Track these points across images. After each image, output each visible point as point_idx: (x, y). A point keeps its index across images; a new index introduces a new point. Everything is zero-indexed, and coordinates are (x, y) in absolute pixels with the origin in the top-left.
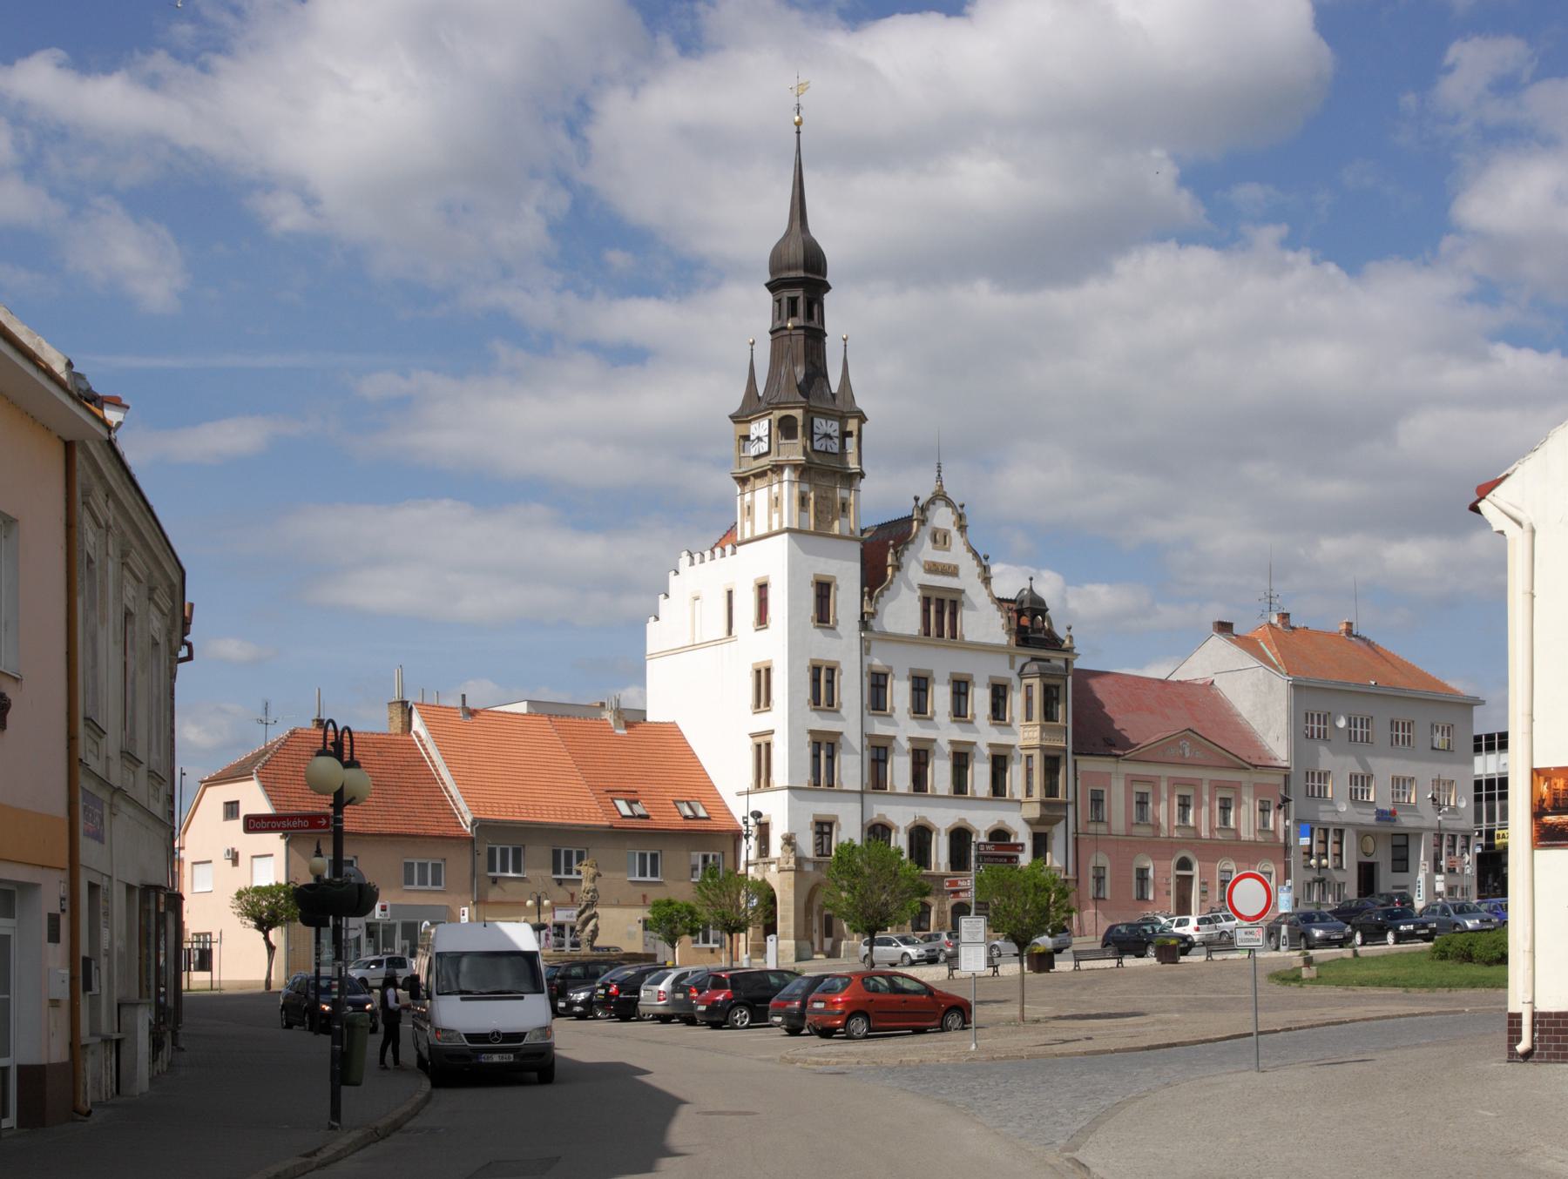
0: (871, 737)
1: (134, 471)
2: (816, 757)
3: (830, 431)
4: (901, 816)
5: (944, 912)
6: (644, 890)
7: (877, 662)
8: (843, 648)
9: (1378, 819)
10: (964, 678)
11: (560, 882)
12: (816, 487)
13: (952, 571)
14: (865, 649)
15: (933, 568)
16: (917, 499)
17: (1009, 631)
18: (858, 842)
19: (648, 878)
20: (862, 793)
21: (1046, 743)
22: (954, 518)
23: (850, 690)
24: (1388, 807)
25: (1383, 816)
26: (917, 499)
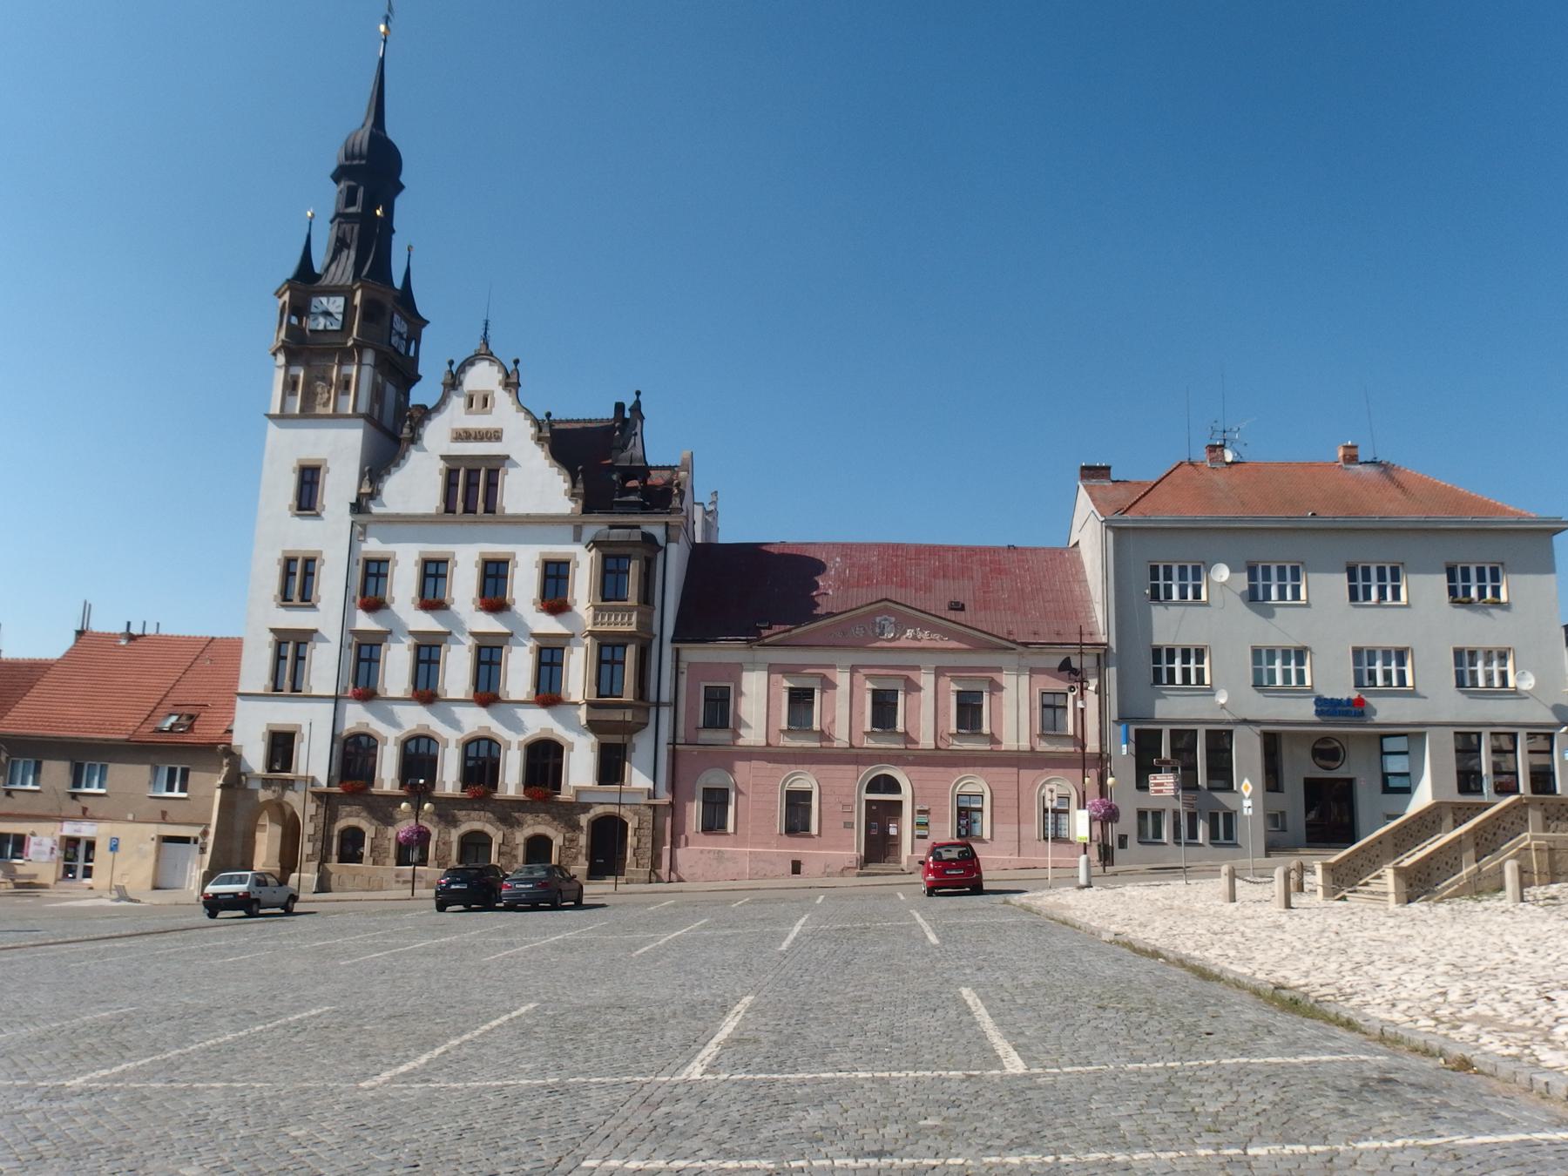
0: (355, 633)
1: (533, 511)
2: (279, 658)
3: (332, 309)
4: (393, 727)
5: (447, 844)
6: (164, 805)
7: (373, 546)
8: (328, 537)
9: (1318, 713)
10: (564, 558)
11: (74, 796)
12: (307, 366)
13: (495, 436)
14: (358, 533)
15: (464, 436)
16: (451, 363)
17: (573, 496)
18: (741, 742)
19: (176, 794)
20: (336, 699)
21: (599, 628)
22: (500, 376)
23: (332, 584)
24: (1344, 690)
25: (1328, 708)
26: (451, 363)
